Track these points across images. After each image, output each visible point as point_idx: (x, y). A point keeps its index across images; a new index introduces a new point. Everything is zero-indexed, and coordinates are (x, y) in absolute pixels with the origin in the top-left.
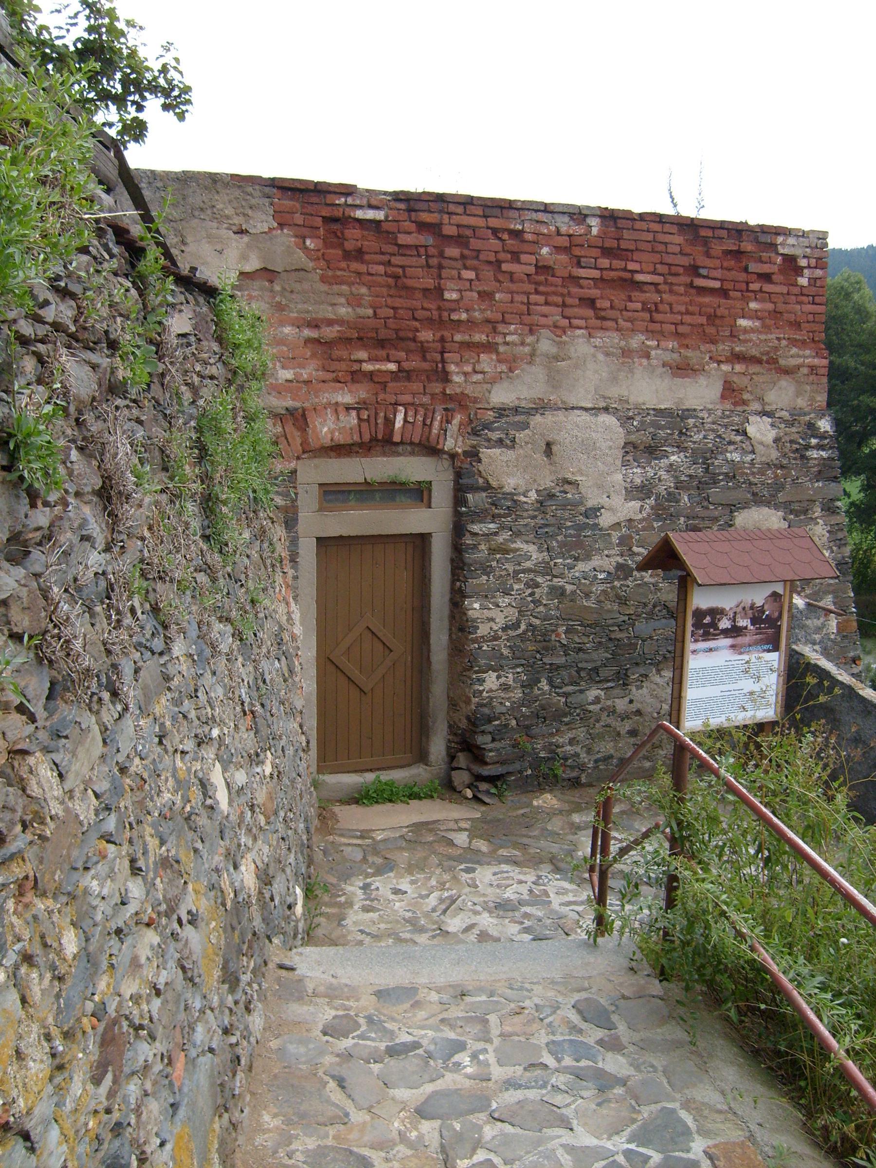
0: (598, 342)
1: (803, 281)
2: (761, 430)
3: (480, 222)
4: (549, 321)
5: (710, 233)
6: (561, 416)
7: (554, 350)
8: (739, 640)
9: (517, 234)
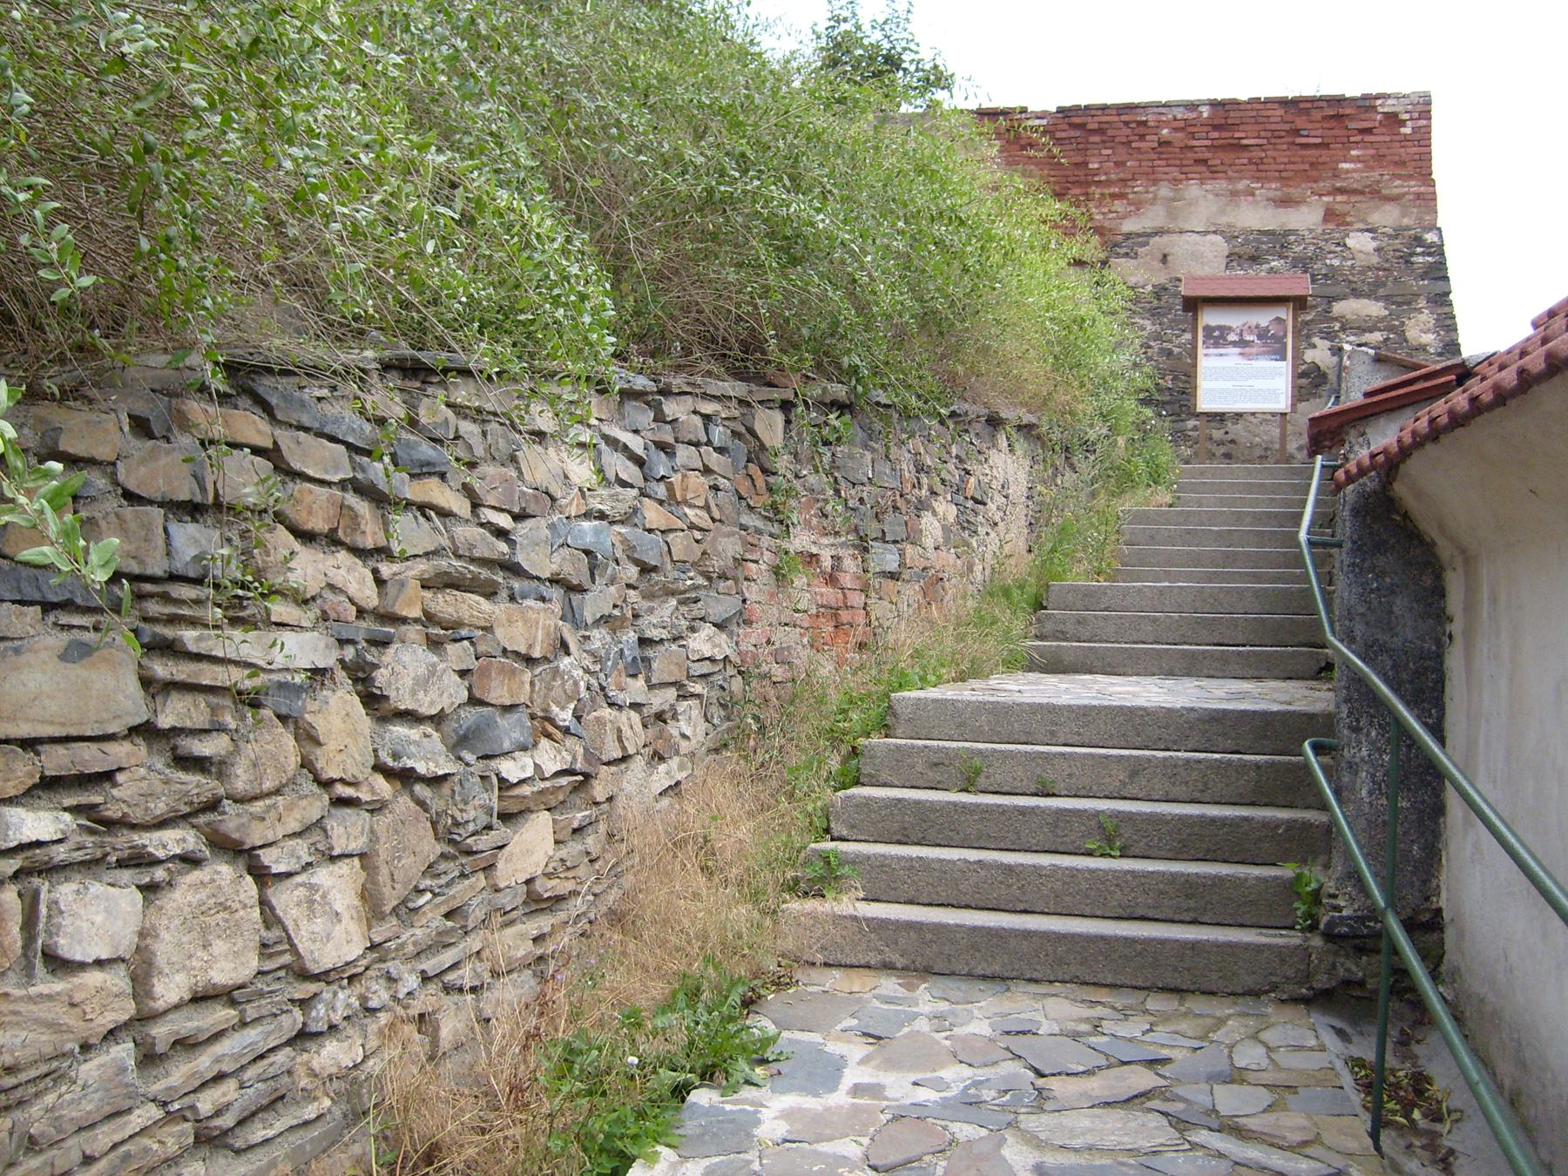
0: (1209, 187)
1: (1407, 130)
2: (1360, 242)
3: (1116, 119)
4: (1170, 177)
5: (1309, 105)
6: (1175, 237)
7: (1171, 195)
8: (1247, 350)
9: (1144, 123)
